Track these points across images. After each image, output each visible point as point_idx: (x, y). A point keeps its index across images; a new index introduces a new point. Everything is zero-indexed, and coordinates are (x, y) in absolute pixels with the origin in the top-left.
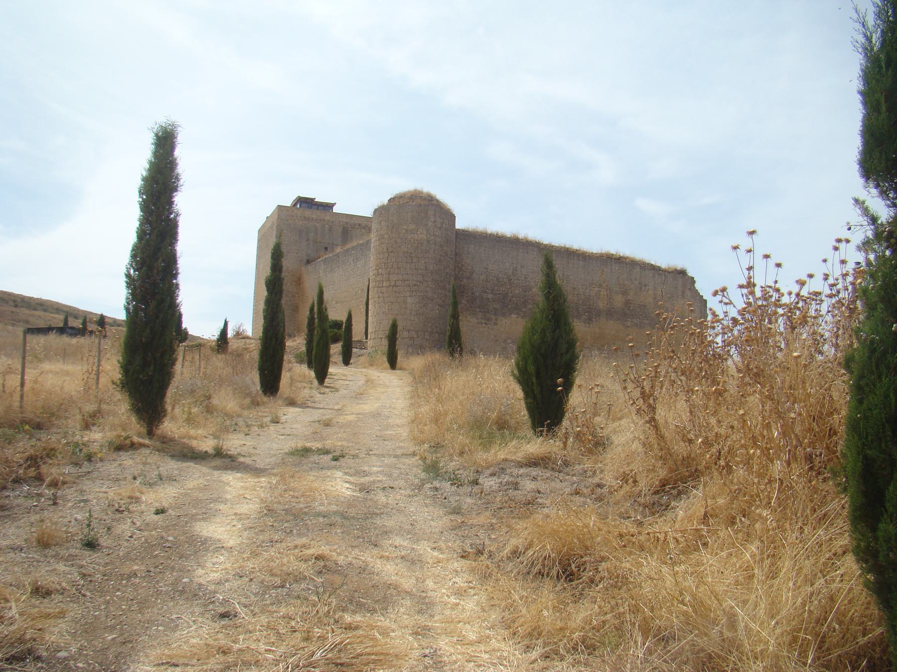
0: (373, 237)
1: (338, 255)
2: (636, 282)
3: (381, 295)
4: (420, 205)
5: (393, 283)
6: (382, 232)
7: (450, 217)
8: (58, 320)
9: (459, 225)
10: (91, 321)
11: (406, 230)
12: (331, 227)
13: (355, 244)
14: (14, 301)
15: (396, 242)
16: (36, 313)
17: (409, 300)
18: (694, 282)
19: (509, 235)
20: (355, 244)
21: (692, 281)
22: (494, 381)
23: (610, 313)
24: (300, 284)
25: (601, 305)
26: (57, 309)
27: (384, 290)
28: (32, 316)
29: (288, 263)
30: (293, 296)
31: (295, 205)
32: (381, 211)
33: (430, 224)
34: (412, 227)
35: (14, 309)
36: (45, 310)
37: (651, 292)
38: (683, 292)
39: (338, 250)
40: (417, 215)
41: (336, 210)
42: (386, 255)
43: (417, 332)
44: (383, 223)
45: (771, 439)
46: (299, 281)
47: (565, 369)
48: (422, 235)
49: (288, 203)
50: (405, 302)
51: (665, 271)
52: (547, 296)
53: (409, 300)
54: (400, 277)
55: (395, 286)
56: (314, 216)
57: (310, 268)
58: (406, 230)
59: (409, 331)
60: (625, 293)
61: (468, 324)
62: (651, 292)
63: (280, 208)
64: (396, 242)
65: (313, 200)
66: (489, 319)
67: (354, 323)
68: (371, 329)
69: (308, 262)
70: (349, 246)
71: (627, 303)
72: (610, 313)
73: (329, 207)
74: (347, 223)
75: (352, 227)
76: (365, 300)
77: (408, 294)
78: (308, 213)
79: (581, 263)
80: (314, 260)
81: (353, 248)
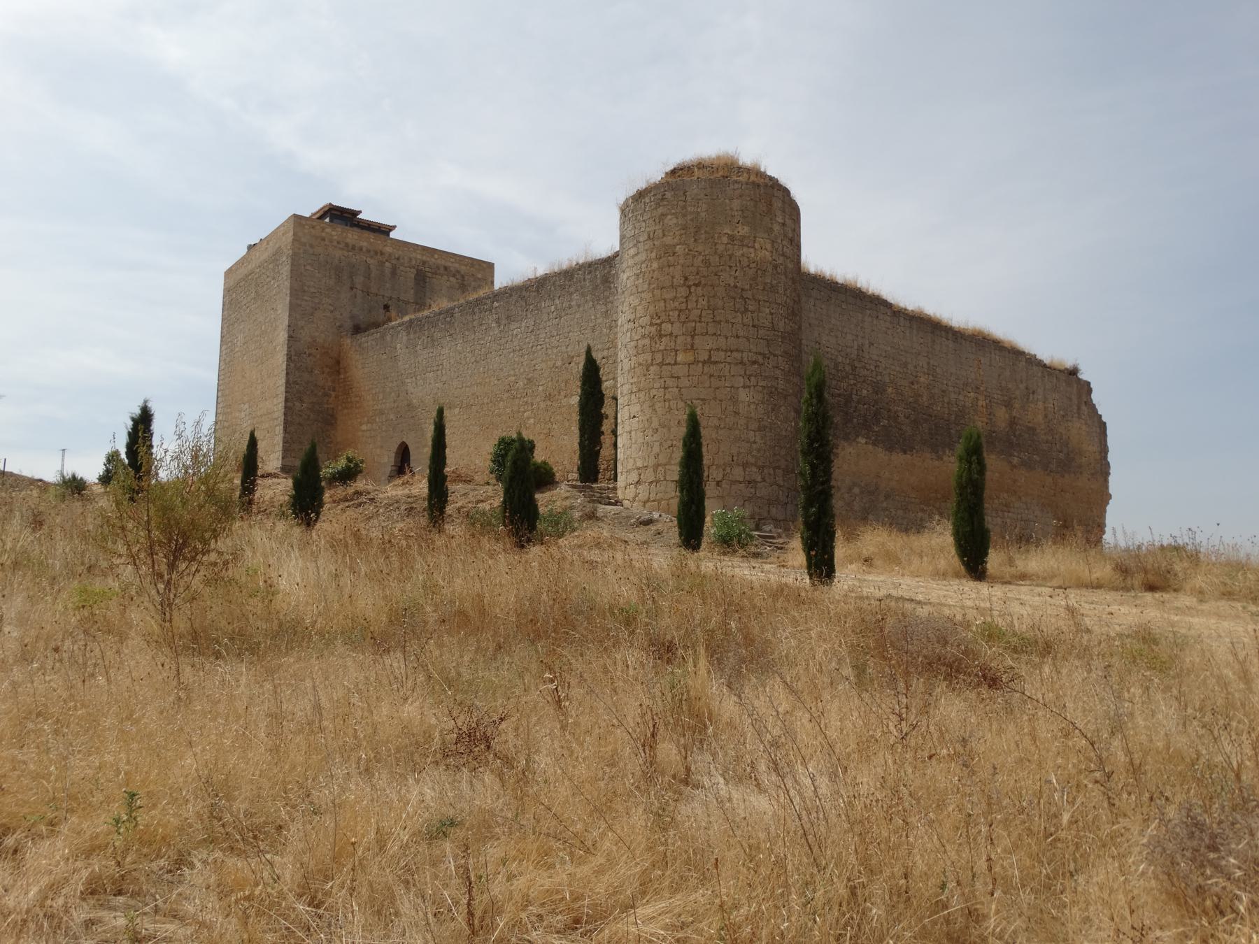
2: (1022, 386)
3: (670, 382)
5: (704, 356)
6: (668, 240)
11: (732, 238)
15: (707, 263)
17: (743, 395)
18: (1090, 391)
21: (1086, 388)
24: (338, 372)
27: (681, 370)
30: (326, 395)
31: (322, 217)
33: (776, 228)
34: (744, 230)
37: (1040, 405)
38: (1079, 408)
42: (683, 291)
43: (761, 468)
44: (670, 221)
50: (734, 400)
53: (743, 395)
54: (722, 342)
55: (709, 361)
56: (365, 244)
57: (367, 340)
58: (732, 238)
59: (745, 466)
60: (1008, 405)
62: (1040, 405)
63: (297, 219)
64: (707, 263)
65: (355, 213)
67: (261, 453)
69: (357, 330)
71: (1013, 422)
73: (383, 231)
74: (424, 263)
77: (740, 381)
79: (951, 344)
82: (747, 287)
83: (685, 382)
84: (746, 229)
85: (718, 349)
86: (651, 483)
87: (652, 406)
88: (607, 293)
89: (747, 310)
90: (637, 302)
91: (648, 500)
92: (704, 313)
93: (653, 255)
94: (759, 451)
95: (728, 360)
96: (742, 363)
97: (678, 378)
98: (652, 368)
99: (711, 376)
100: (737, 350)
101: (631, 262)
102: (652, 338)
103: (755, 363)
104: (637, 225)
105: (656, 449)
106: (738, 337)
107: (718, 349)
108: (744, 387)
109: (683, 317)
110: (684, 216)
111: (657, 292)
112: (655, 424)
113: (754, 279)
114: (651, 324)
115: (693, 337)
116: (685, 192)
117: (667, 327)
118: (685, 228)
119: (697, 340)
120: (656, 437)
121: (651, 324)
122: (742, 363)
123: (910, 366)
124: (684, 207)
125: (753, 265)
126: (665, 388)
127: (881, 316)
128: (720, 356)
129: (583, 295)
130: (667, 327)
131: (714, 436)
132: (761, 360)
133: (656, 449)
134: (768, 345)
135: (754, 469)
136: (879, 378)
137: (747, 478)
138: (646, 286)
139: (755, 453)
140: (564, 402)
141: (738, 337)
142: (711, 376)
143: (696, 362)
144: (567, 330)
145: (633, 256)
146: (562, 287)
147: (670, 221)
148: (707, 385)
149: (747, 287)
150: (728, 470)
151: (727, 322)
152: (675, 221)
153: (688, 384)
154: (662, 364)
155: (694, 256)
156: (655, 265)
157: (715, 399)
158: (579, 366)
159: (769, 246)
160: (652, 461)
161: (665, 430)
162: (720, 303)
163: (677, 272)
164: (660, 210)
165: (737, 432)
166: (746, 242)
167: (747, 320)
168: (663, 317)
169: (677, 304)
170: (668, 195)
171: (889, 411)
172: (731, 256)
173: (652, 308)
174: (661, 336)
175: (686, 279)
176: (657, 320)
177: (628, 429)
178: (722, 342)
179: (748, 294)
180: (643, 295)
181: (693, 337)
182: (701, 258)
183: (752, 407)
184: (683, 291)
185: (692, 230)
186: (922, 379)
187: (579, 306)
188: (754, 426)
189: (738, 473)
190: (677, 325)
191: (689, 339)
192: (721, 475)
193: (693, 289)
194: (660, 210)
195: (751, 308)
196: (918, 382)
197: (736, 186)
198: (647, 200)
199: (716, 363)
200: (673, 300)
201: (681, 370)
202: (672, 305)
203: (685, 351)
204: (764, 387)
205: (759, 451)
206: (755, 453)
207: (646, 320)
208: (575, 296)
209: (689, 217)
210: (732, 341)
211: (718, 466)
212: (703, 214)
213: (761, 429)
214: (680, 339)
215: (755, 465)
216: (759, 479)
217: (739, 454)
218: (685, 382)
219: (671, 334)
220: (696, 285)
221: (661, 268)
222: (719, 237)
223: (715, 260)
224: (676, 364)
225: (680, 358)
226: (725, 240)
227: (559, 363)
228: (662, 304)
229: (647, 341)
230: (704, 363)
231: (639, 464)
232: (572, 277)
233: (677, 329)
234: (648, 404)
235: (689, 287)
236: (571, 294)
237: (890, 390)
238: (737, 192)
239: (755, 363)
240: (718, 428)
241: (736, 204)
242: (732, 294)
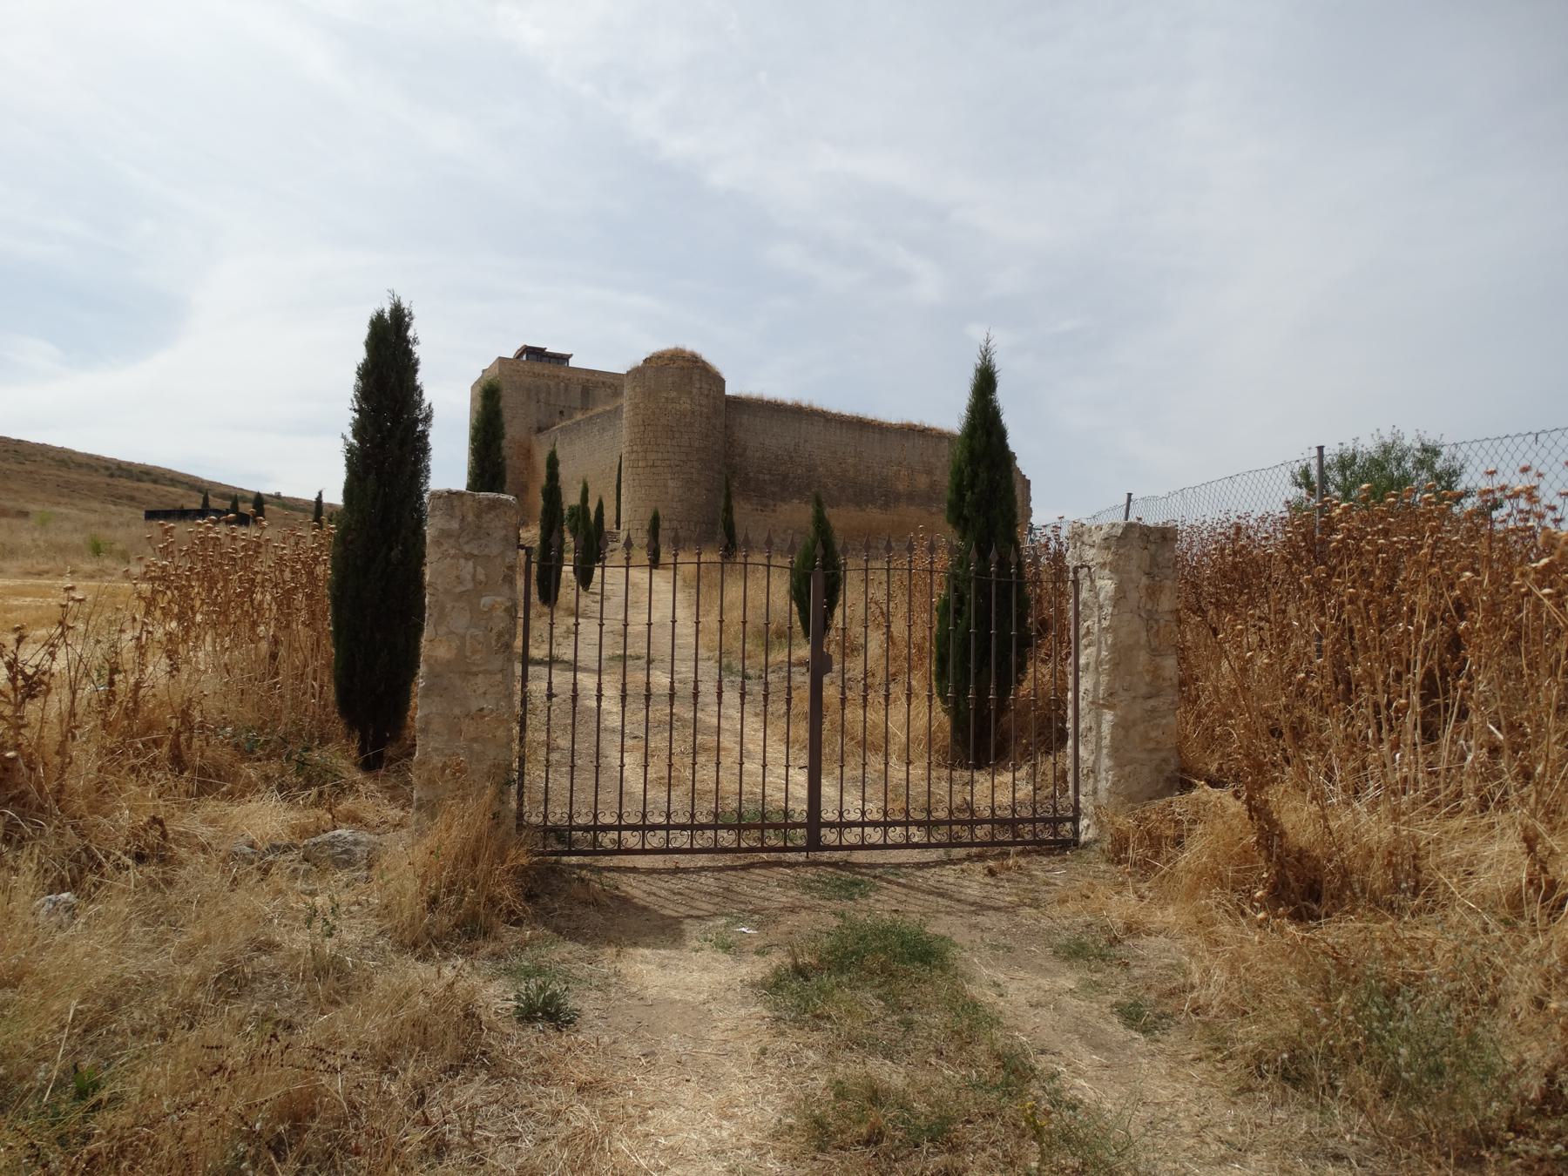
0: (625, 402)
1: (578, 423)
4: (682, 368)
7: (720, 382)
8: (195, 503)
9: (729, 391)
10: (245, 500)
12: (567, 386)
13: (599, 409)
14: (107, 468)
16: (142, 485)
17: (670, 483)
19: (789, 402)
20: (599, 409)
22: (768, 591)
23: (911, 497)
25: (901, 487)
26: (172, 480)
28: (138, 489)
29: (514, 430)
31: (519, 356)
32: (636, 372)
34: (674, 394)
35: (109, 480)
36: (155, 482)
39: (579, 416)
40: (682, 373)
41: (572, 363)
46: (528, 454)
47: (832, 590)
48: (685, 404)
49: (510, 354)
50: (665, 486)
52: (817, 528)
53: (670, 483)
55: (653, 466)
57: (542, 437)
61: (744, 513)
65: (543, 350)
66: (766, 506)
68: (627, 517)
69: (540, 430)
70: (591, 413)
72: (911, 497)
73: (563, 359)
75: (595, 386)
76: (615, 483)
78: (538, 367)
79: (877, 436)
80: (548, 428)
81: (598, 416)
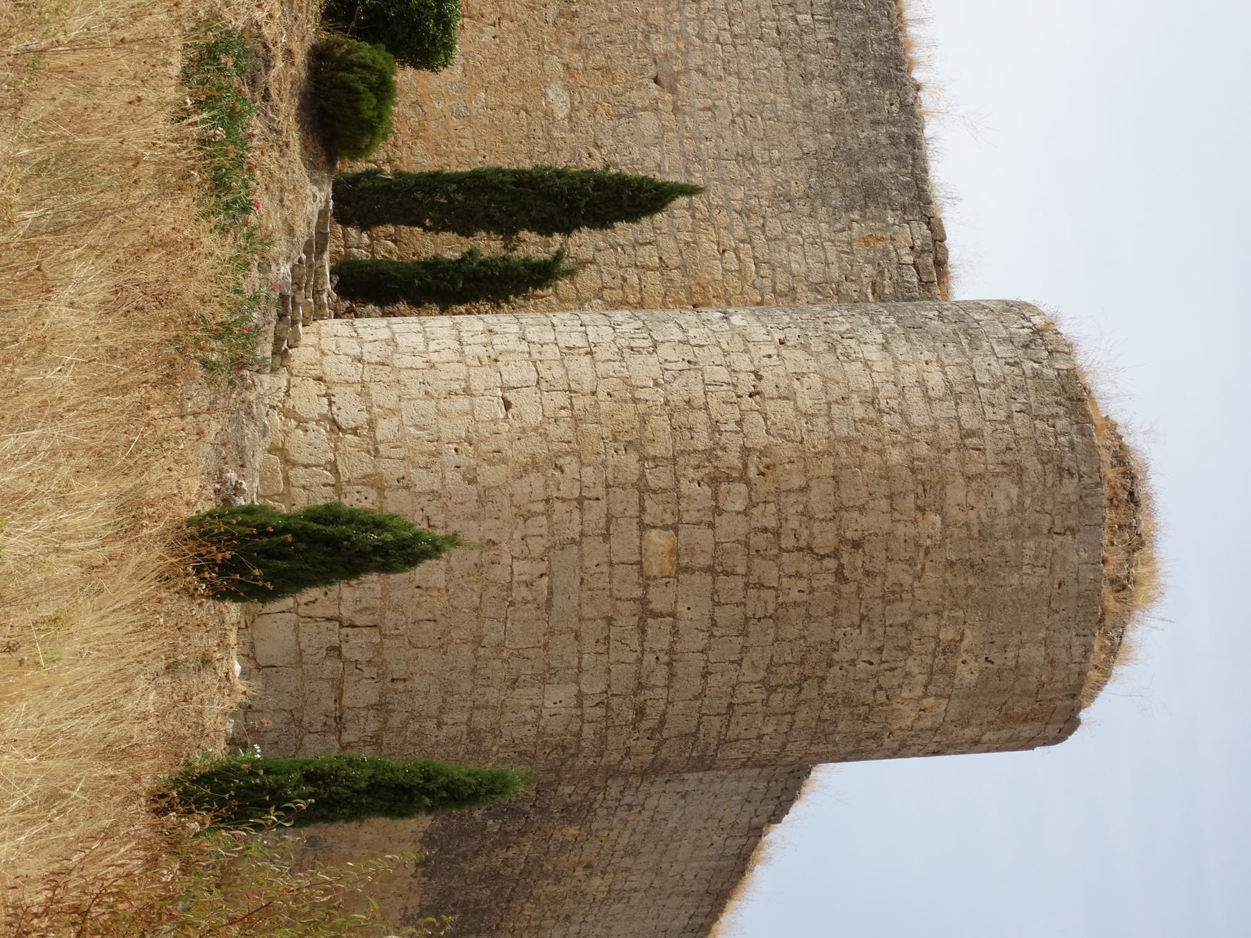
3: (595, 513)
5: (659, 599)
6: (957, 492)
11: (951, 649)
15: (893, 595)
17: (559, 696)
27: (624, 544)
34: (968, 673)
42: (825, 538)
44: (1005, 493)
45: (533, 846)
50: (546, 676)
51: (756, 833)
53: (559, 696)
54: (694, 640)
55: (646, 612)
59: (381, 707)
64: (893, 595)
77: (593, 686)
82: (828, 688)
83: (595, 553)
84: (971, 679)
85: (675, 632)
86: (333, 467)
87: (534, 464)
88: (836, 198)
89: (771, 690)
90: (805, 402)
91: (288, 461)
92: (769, 595)
93: (923, 450)
94: (420, 734)
95: (649, 658)
96: (640, 686)
97: (606, 537)
98: (632, 458)
99: (609, 620)
100: (672, 676)
101: (908, 374)
102: (710, 454)
103: (640, 712)
104: (1001, 394)
105: (424, 480)
106: (706, 675)
107: (675, 632)
108: (580, 696)
109: (759, 541)
110: (1015, 532)
111: (826, 466)
112: (490, 475)
113: (847, 700)
114: (746, 451)
115: (710, 569)
116: (1073, 531)
117: (735, 498)
118: (985, 534)
119: (701, 582)
120: (454, 479)
121: (746, 451)
122: (640, 686)
123: (629, 861)
124: (1035, 531)
125: (881, 697)
126: (580, 500)
127: (749, 808)
128: (658, 635)
129: (836, 120)
130: (735, 498)
131: (455, 634)
132: (646, 724)
133: (424, 480)
134: (683, 736)
135: (372, 727)
136: (602, 812)
137: (348, 715)
138: (843, 430)
139: (414, 726)
140: (554, 64)
141: (706, 675)
142: (609, 620)
143: (646, 580)
144: (746, 67)
145: (922, 383)
146: (860, 50)
147: (1005, 493)
148: (588, 612)
149: (828, 688)
150: (370, 672)
151: (745, 649)
152: (1004, 507)
153: (590, 563)
154: (643, 488)
155: (911, 562)
156: (896, 456)
157: (551, 632)
158: (639, 155)
159: (927, 723)
160: (391, 469)
161: (472, 506)
162: (791, 632)
163: (875, 521)
164: (1032, 464)
165: (466, 686)
166: (940, 680)
167: (745, 692)
168: (763, 487)
169: (794, 523)
170: (1070, 487)
171: (522, 833)
172: (906, 649)
173: (787, 450)
174: (714, 481)
175: (857, 545)
176: (753, 470)
177: (477, 385)
178: (694, 640)
179: (810, 691)
180: (821, 422)
181: (710, 569)
182: (907, 580)
183: (530, 715)
184: (825, 538)
185: (978, 554)
186: (597, 881)
187: (807, 107)
188: (482, 720)
189: (362, 693)
190: (741, 527)
191: (704, 560)
192: (356, 655)
193: (831, 563)
194: (1032, 464)
195: (776, 698)
196: (589, 876)
197: (1077, 652)
198: (1062, 424)
199: (643, 630)
200: (807, 514)
201: (624, 544)
202: (792, 506)
203: (675, 552)
204: (578, 734)
205: (420, 734)
206: (414, 726)
207: (759, 438)
208: (834, 92)
209: (1009, 545)
210: (698, 662)
211: (378, 648)
212: (1014, 580)
213: (474, 734)
214: (704, 537)
215: (384, 726)
216: (347, 737)
217: (410, 693)
218: (595, 553)
219: (718, 511)
220: (839, 573)
221: (887, 473)
222: (955, 620)
223: (900, 612)
224: (643, 527)
225: (657, 538)
226: (948, 634)
227: (659, 45)
228: (797, 481)
229: (702, 440)
230: (644, 602)
231: (385, 429)
232: (885, 80)
233: (732, 527)
234: (541, 449)
235: (836, 554)
236: (840, 80)
237: (574, 831)
238: (1062, 656)
239: (640, 712)
240: (478, 641)
241: (1036, 654)
242: (813, 657)
